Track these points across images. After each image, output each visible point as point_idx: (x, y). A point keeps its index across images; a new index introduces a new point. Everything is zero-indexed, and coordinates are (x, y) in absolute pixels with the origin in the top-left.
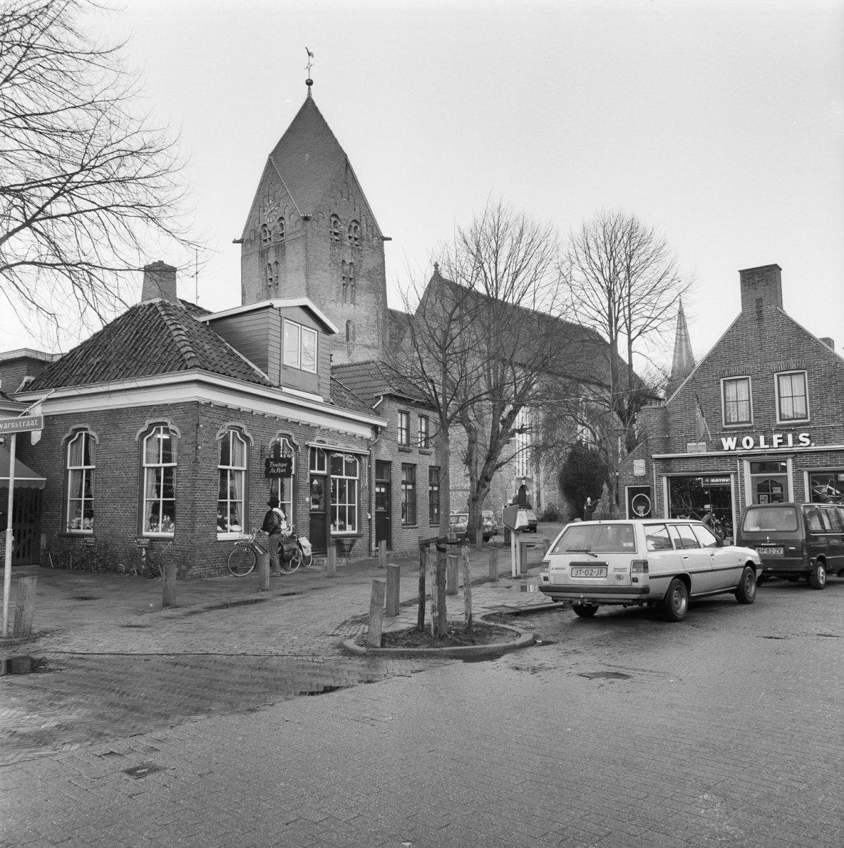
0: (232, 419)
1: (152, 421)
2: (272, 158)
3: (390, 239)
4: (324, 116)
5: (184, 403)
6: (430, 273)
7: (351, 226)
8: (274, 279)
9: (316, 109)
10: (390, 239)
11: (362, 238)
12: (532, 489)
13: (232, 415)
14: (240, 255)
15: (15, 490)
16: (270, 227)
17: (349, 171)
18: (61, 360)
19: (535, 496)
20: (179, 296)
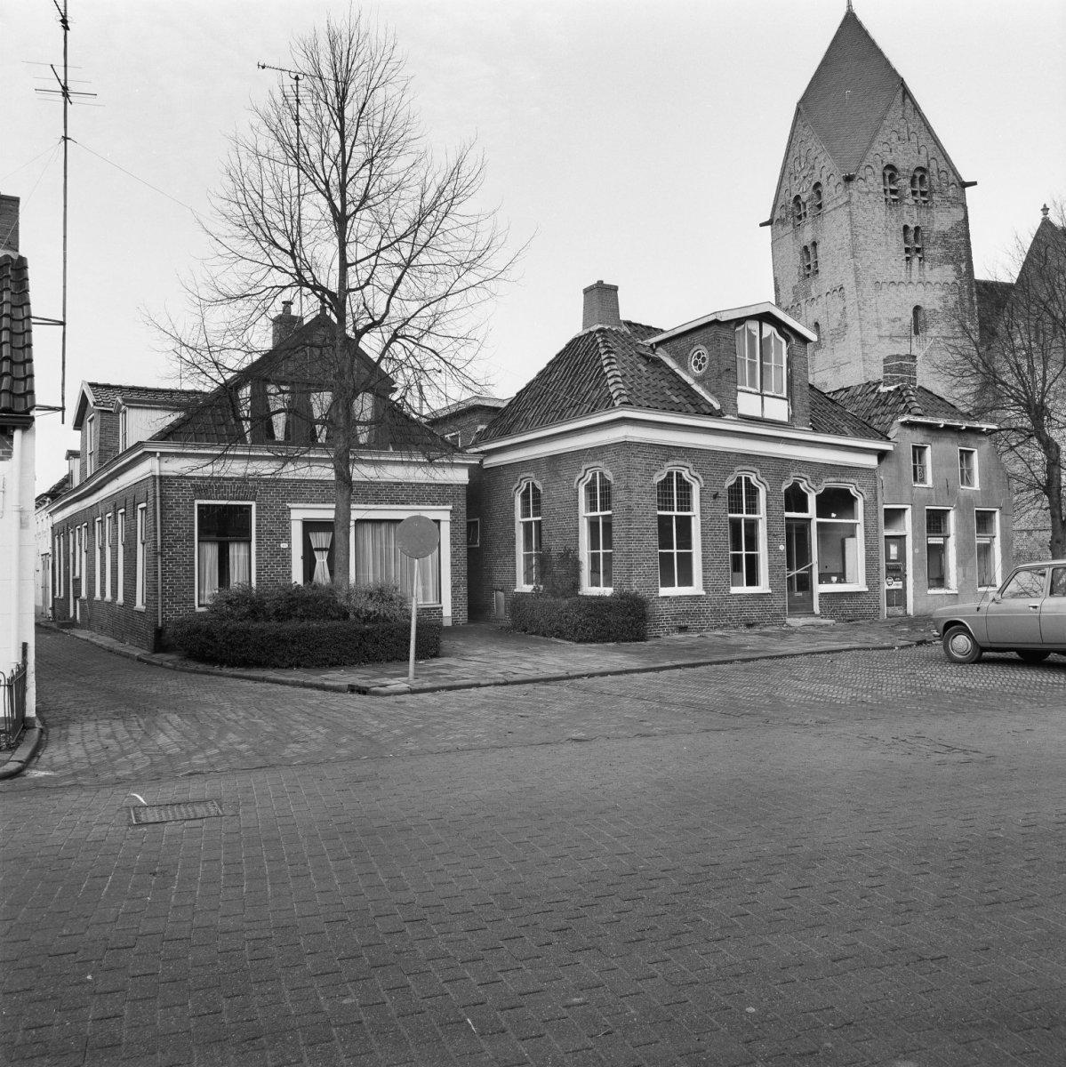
0: (674, 458)
1: (587, 466)
4: (876, 41)
5: (616, 443)
7: (914, 177)
8: (812, 265)
9: (865, 34)
11: (932, 191)
13: (674, 453)
14: (770, 240)
15: (754, 555)
16: (804, 198)
18: (510, 404)
20: (623, 317)
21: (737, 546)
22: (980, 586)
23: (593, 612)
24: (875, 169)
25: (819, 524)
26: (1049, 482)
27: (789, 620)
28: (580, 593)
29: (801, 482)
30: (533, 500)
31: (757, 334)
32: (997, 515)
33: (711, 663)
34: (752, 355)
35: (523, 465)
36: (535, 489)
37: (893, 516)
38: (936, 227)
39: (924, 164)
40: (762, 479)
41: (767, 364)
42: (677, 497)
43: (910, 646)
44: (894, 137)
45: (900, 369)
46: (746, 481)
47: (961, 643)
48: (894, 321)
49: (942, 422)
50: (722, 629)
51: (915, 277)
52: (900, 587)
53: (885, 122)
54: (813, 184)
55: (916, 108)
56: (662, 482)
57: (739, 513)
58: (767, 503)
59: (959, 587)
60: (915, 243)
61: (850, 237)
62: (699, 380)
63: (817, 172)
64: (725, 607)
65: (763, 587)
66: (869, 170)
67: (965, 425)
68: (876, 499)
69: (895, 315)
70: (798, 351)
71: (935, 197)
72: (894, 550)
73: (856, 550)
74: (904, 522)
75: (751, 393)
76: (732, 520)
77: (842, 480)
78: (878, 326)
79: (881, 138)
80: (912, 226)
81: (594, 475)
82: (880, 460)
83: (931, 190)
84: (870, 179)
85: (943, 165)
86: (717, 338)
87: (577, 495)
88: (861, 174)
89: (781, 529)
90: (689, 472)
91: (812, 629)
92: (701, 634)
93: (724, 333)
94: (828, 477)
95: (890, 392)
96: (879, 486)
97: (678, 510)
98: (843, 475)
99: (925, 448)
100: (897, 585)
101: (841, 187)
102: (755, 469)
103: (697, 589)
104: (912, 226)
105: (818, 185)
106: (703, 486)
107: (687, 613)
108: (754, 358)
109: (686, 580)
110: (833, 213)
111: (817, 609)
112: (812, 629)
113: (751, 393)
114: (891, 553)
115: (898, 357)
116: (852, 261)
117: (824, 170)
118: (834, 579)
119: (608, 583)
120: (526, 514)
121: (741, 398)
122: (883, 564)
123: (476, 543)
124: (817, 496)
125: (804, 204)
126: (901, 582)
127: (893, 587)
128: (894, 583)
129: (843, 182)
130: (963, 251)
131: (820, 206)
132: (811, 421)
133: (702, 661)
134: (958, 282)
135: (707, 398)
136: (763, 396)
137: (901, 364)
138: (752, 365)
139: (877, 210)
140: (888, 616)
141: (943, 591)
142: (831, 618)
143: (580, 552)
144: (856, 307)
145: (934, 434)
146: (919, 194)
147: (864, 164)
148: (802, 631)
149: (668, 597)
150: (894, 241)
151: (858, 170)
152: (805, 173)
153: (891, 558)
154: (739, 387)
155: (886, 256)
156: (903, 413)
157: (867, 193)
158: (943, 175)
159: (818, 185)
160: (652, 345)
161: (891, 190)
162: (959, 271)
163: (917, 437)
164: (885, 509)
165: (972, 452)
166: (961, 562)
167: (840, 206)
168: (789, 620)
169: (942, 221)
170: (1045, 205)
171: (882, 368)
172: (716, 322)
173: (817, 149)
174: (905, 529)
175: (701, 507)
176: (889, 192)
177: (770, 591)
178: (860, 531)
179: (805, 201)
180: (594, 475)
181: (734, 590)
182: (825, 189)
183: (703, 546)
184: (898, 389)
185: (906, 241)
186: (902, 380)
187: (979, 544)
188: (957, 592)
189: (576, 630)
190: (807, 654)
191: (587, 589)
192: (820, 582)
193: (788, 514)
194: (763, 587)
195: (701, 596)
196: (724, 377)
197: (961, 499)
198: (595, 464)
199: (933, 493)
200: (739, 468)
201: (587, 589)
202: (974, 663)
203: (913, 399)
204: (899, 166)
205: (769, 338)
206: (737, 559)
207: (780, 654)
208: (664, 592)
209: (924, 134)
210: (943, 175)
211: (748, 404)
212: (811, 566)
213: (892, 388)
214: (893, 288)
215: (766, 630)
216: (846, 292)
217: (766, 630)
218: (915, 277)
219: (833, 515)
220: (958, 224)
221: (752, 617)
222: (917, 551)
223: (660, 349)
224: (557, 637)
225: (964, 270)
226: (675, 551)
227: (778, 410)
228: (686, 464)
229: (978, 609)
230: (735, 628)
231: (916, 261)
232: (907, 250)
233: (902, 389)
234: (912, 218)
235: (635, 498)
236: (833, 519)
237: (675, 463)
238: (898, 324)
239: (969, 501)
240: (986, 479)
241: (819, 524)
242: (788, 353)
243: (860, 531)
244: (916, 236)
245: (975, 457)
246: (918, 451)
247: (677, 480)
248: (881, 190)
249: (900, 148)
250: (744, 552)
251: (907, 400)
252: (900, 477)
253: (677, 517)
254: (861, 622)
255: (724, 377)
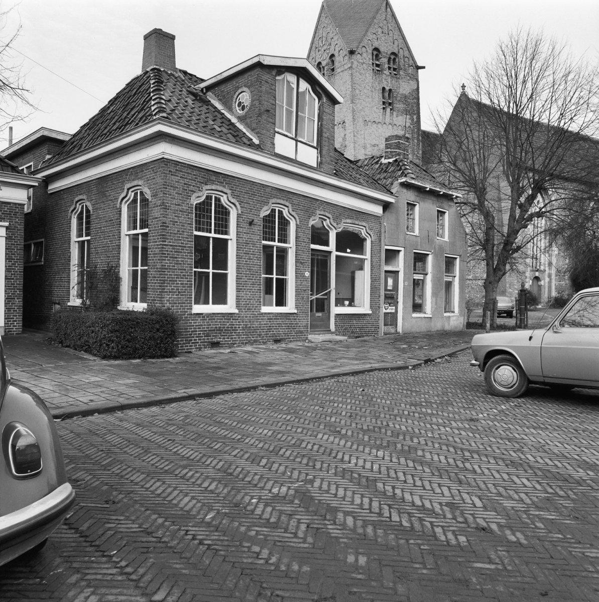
2: (325, 5)
3: (424, 67)
6: (459, 91)
10: (424, 67)
12: (544, 279)
13: (213, 178)
15: (283, 279)
16: (324, 63)
17: (389, 9)
19: (547, 284)
21: (269, 271)
22: (445, 312)
23: (117, 328)
24: (368, 49)
25: (337, 257)
26: (487, 240)
27: (310, 337)
28: (119, 308)
29: (325, 220)
30: (87, 222)
31: (295, 86)
32: (458, 260)
33: (232, 391)
34: (290, 104)
35: (78, 187)
36: (88, 211)
37: (391, 255)
38: (401, 91)
39: (396, 51)
40: (293, 213)
41: (301, 114)
42: (215, 220)
43: (420, 365)
44: (380, 30)
45: (398, 146)
46: (279, 213)
47: (505, 374)
48: (374, 146)
49: (428, 186)
50: (252, 344)
51: (388, 120)
52: (393, 311)
53: (375, 21)
54: (330, 55)
55: (393, 16)
56: (200, 204)
57: (272, 241)
58: (296, 234)
59: (433, 313)
60: (388, 99)
61: (350, 90)
62: (241, 119)
63: (332, 47)
64: (256, 324)
65: (290, 307)
66: (364, 49)
67: (443, 191)
68: (380, 241)
69: (377, 143)
70: (327, 110)
71: (401, 73)
72: (390, 282)
73: (363, 280)
74: (399, 261)
75: (286, 136)
76: (265, 247)
77: (357, 223)
78: (365, 148)
79: (372, 30)
80: (387, 88)
81: (136, 194)
82: (384, 210)
83: (399, 67)
84: (365, 55)
85: (407, 54)
86: (259, 81)
87: (120, 214)
88: (359, 51)
89: (307, 257)
90: (228, 197)
91: (330, 345)
92: (232, 349)
93: (266, 76)
94: (346, 218)
95: (389, 163)
96: (383, 231)
97: (215, 233)
98: (357, 219)
99: (415, 205)
100: (391, 310)
101: (347, 58)
102: (287, 204)
103: (230, 307)
104: (387, 88)
105: (333, 56)
106: (240, 212)
107: (220, 330)
108: (291, 107)
109: (221, 298)
110: (341, 74)
111: (332, 327)
112: (330, 345)
113: (286, 136)
114: (389, 284)
115: (397, 137)
116: (351, 105)
117: (337, 46)
118: (347, 303)
119: (143, 300)
120: (80, 235)
121: (278, 139)
122: (382, 293)
123: (41, 261)
124: (337, 234)
125: (323, 67)
126: (394, 307)
127: (388, 311)
128: (390, 307)
129: (348, 54)
130: (415, 108)
131: (333, 70)
132: (336, 170)
133: (221, 388)
134: (412, 127)
135: (248, 134)
136: (297, 141)
137: (399, 142)
138: (289, 113)
139: (367, 75)
140: (385, 334)
141: (422, 315)
142: (344, 335)
143: (121, 269)
144: (352, 134)
145: (421, 195)
146: (392, 69)
147: (361, 44)
148: (324, 348)
149: (202, 314)
150: (377, 96)
151: (358, 48)
152: (325, 47)
153: (389, 288)
154: (277, 130)
155: (372, 104)
156: (401, 176)
157: (363, 64)
158: (406, 59)
159: (333, 56)
160: (202, 89)
161: (376, 64)
162: (413, 120)
163: (410, 196)
164: (386, 250)
165: (445, 213)
166: (435, 294)
167: (346, 70)
168: (310, 337)
169: (405, 88)
170: (463, 84)
171: (384, 145)
172: (259, 65)
173: (333, 33)
174: (398, 266)
175: (237, 232)
176: (375, 65)
177: (296, 311)
178: (367, 266)
179: (324, 65)
180: (136, 194)
181: (265, 309)
182: (337, 59)
183: (238, 268)
184: (396, 161)
185: (383, 97)
186: (399, 154)
187: (446, 281)
188: (431, 316)
189: (101, 345)
190: (333, 376)
191: (127, 304)
192: (336, 305)
193: (313, 246)
194: (290, 307)
195: (234, 313)
196: (264, 117)
197: (437, 247)
198: (135, 183)
199: (419, 239)
200: (274, 200)
201: (127, 304)
202: (519, 397)
203: (408, 167)
204: (382, 49)
205: (304, 93)
206: (269, 282)
207: (307, 376)
208: (197, 309)
209: (397, 33)
210: (406, 59)
211: (283, 145)
212: (330, 292)
213: (391, 160)
214: (375, 125)
215: (291, 345)
216: (347, 125)
217: (291, 345)
218: (388, 120)
219: (349, 250)
220: (413, 91)
221: (279, 333)
222: (406, 283)
223: (209, 94)
224: (86, 351)
225: (415, 120)
226: (211, 271)
227: (309, 156)
228: (225, 190)
229: (531, 338)
230: (264, 343)
231: (388, 110)
232: (384, 103)
233: (399, 160)
234: (388, 83)
235: (171, 216)
236: (348, 254)
237: (214, 187)
238: (376, 148)
239: (441, 249)
240: (452, 235)
241: (337, 257)
242: (319, 109)
243: (367, 266)
244: (389, 95)
245: (447, 215)
246: (411, 206)
247: (215, 204)
248: (371, 63)
249: (383, 38)
250: (275, 276)
251: (403, 168)
252: (397, 225)
253: (214, 238)
254: (365, 338)
255: (263, 117)
